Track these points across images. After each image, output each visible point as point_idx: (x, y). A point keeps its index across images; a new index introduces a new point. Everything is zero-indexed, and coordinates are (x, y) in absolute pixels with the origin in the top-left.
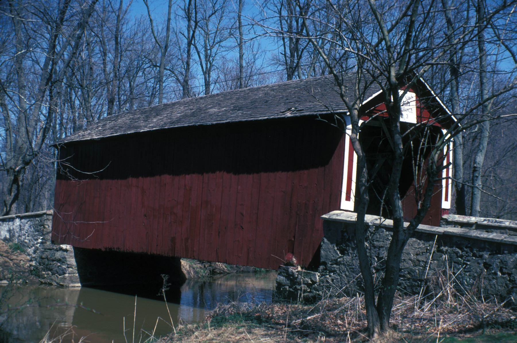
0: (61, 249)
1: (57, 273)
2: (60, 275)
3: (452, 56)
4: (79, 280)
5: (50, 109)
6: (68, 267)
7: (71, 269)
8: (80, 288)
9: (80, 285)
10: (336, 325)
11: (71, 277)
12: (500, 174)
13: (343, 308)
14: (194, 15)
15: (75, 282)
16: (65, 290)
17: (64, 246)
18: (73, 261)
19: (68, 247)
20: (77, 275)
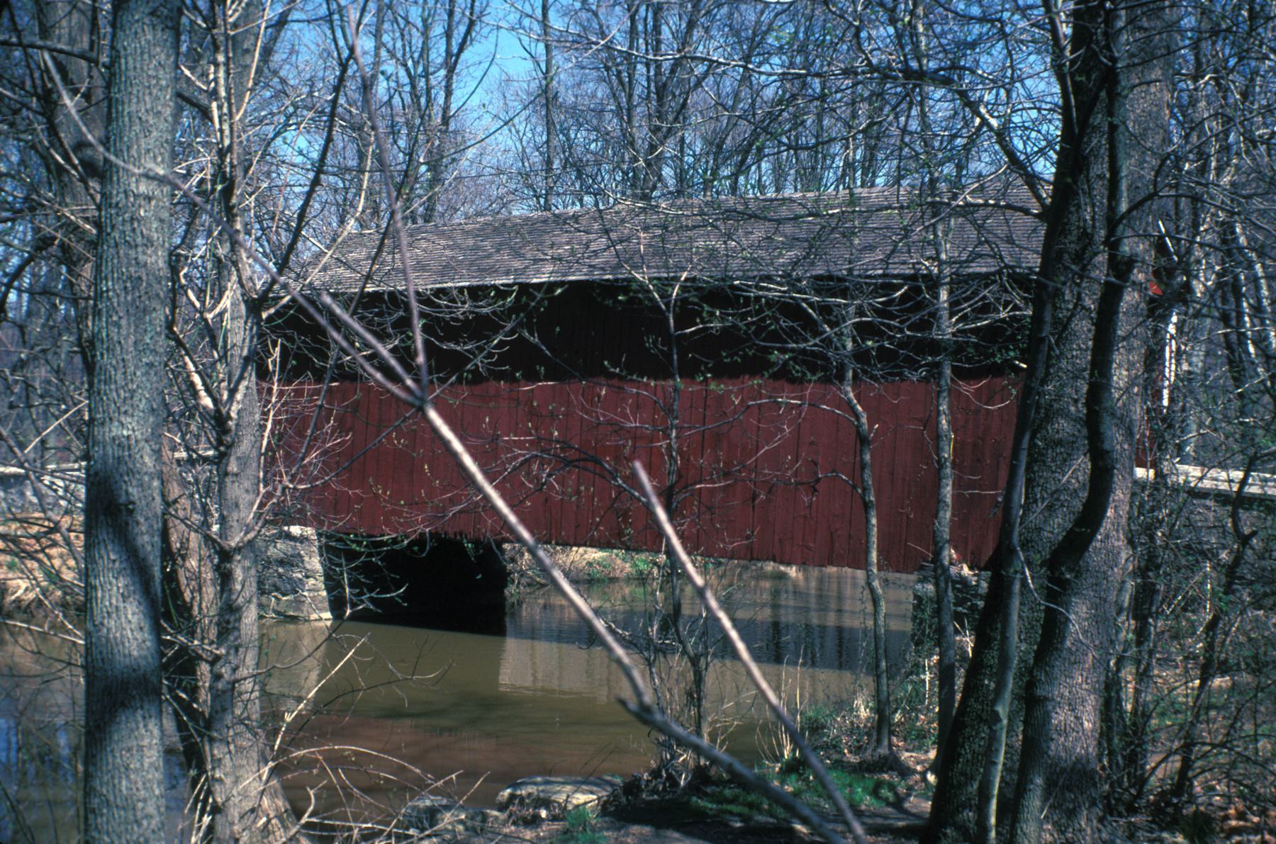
0: (289, 536)
1: (277, 589)
2: (284, 595)
3: (839, 765)
4: (327, 604)
5: (877, 696)
6: (307, 577)
7: (312, 581)
8: (329, 623)
9: (328, 615)
10: (818, 115)
11: (313, 598)
12: (1068, 310)
13: (275, 500)
14: (441, 100)
15: (321, 610)
16: (304, 628)
17: (295, 530)
18: (315, 563)
19: (310, 531)
20: (324, 593)
